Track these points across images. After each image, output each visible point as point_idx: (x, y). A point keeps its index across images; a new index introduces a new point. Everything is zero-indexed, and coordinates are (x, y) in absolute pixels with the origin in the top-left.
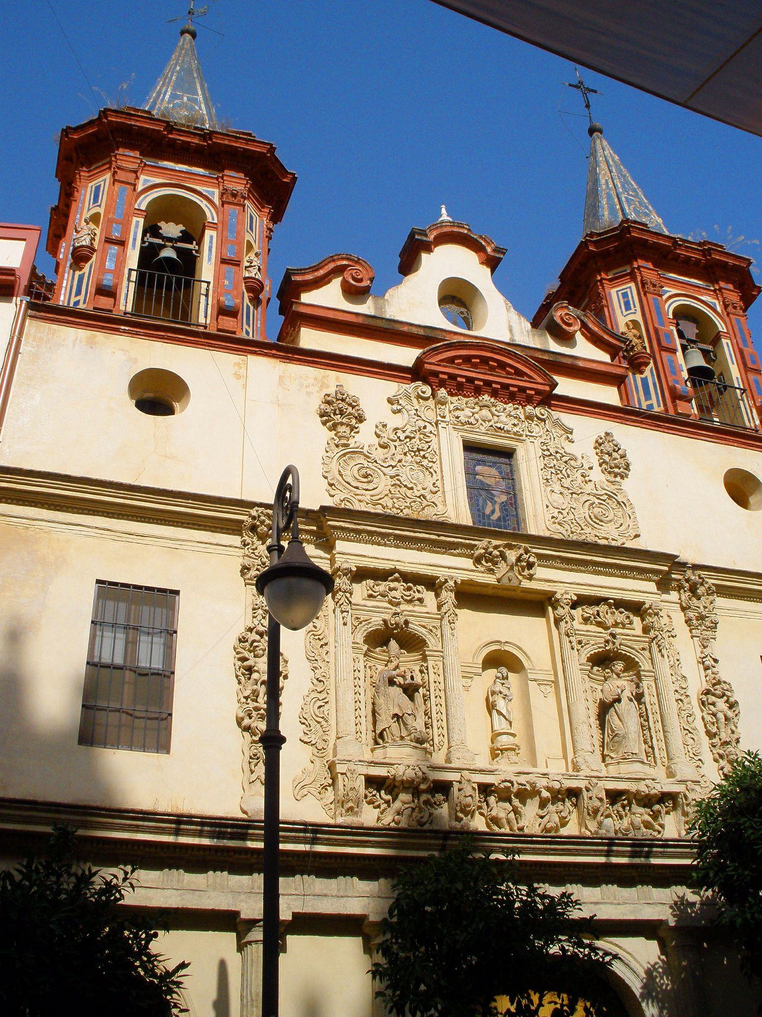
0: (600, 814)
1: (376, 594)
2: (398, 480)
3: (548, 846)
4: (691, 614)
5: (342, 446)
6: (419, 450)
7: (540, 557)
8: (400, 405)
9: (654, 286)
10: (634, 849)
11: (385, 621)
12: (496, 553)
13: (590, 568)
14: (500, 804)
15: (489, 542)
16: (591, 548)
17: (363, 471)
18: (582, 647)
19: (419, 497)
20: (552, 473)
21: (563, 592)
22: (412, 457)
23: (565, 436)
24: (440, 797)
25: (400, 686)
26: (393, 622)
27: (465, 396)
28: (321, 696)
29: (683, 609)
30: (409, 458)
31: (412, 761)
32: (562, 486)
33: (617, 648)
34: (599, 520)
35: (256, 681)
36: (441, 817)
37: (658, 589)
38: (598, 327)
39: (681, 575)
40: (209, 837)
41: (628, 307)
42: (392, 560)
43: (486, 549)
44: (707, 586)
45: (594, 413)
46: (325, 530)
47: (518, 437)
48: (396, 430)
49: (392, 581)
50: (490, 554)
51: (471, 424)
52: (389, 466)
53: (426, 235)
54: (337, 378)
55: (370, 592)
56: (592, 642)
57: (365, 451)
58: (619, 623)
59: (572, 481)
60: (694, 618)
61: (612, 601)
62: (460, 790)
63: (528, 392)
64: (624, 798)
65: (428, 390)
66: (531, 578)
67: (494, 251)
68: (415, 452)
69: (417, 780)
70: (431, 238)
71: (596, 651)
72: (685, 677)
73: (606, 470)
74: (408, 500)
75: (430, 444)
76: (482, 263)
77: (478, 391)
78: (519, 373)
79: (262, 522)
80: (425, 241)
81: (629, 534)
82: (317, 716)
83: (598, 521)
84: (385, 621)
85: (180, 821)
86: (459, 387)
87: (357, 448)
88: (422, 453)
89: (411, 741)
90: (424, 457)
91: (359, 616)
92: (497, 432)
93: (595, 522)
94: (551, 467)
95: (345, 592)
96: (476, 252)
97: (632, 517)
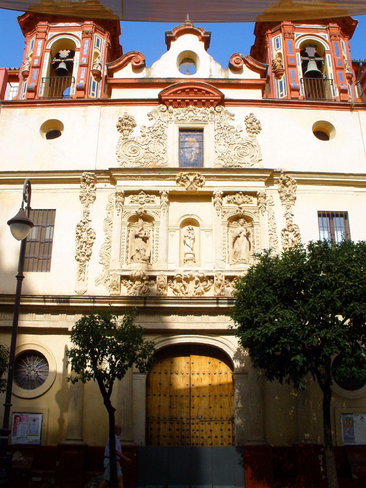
0: (221, 286)
1: (133, 201)
2: (149, 150)
3: (189, 301)
4: (282, 194)
6: (159, 135)
7: (206, 177)
8: (152, 116)
9: (289, 34)
10: (229, 301)
11: (136, 212)
12: (185, 178)
13: (231, 179)
14: (178, 283)
15: (182, 174)
19: (157, 156)
20: (221, 136)
21: (216, 191)
22: (156, 139)
24: (153, 282)
25: (141, 238)
27: (182, 107)
28: (108, 245)
30: (154, 139)
31: (140, 269)
35: (81, 242)
36: (154, 290)
37: (265, 185)
38: (253, 62)
40: (56, 302)
41: (278, 47)
44: (291, 181)
47: (205, 122)
49: (141, 194)
50: (182, 178)
51: (183, 120)
53: (172, 34)
56: (231, 211)
57: (135, 140)
58: (245, 202)
61: (241, 192)
62: (159, 279)
63: (211, 101)
64: (235, 279)
65: (165, 107)
66: (202, 186)
67: (205, 34)
68: (157, 136)
69: (141, 276)
70: (174, 34)
71: (232, 215)
73: (248, 131)
74: (152, 158)
75: (164, 132)
76: (200, 41)
77: (187, 104)
78: (208, 93)
79: (87, 178)
80: (171, 36)
83: (241, 156)
84: (136, 212)
85: (45, 298)
86: (177, 104)
87: (132, 139)
88: (160, 136)
90: (161, 138)
92: (195, 121)
93: (240, 156)
94: (221, 134)
95: (119, 202)
96: (198, 36)
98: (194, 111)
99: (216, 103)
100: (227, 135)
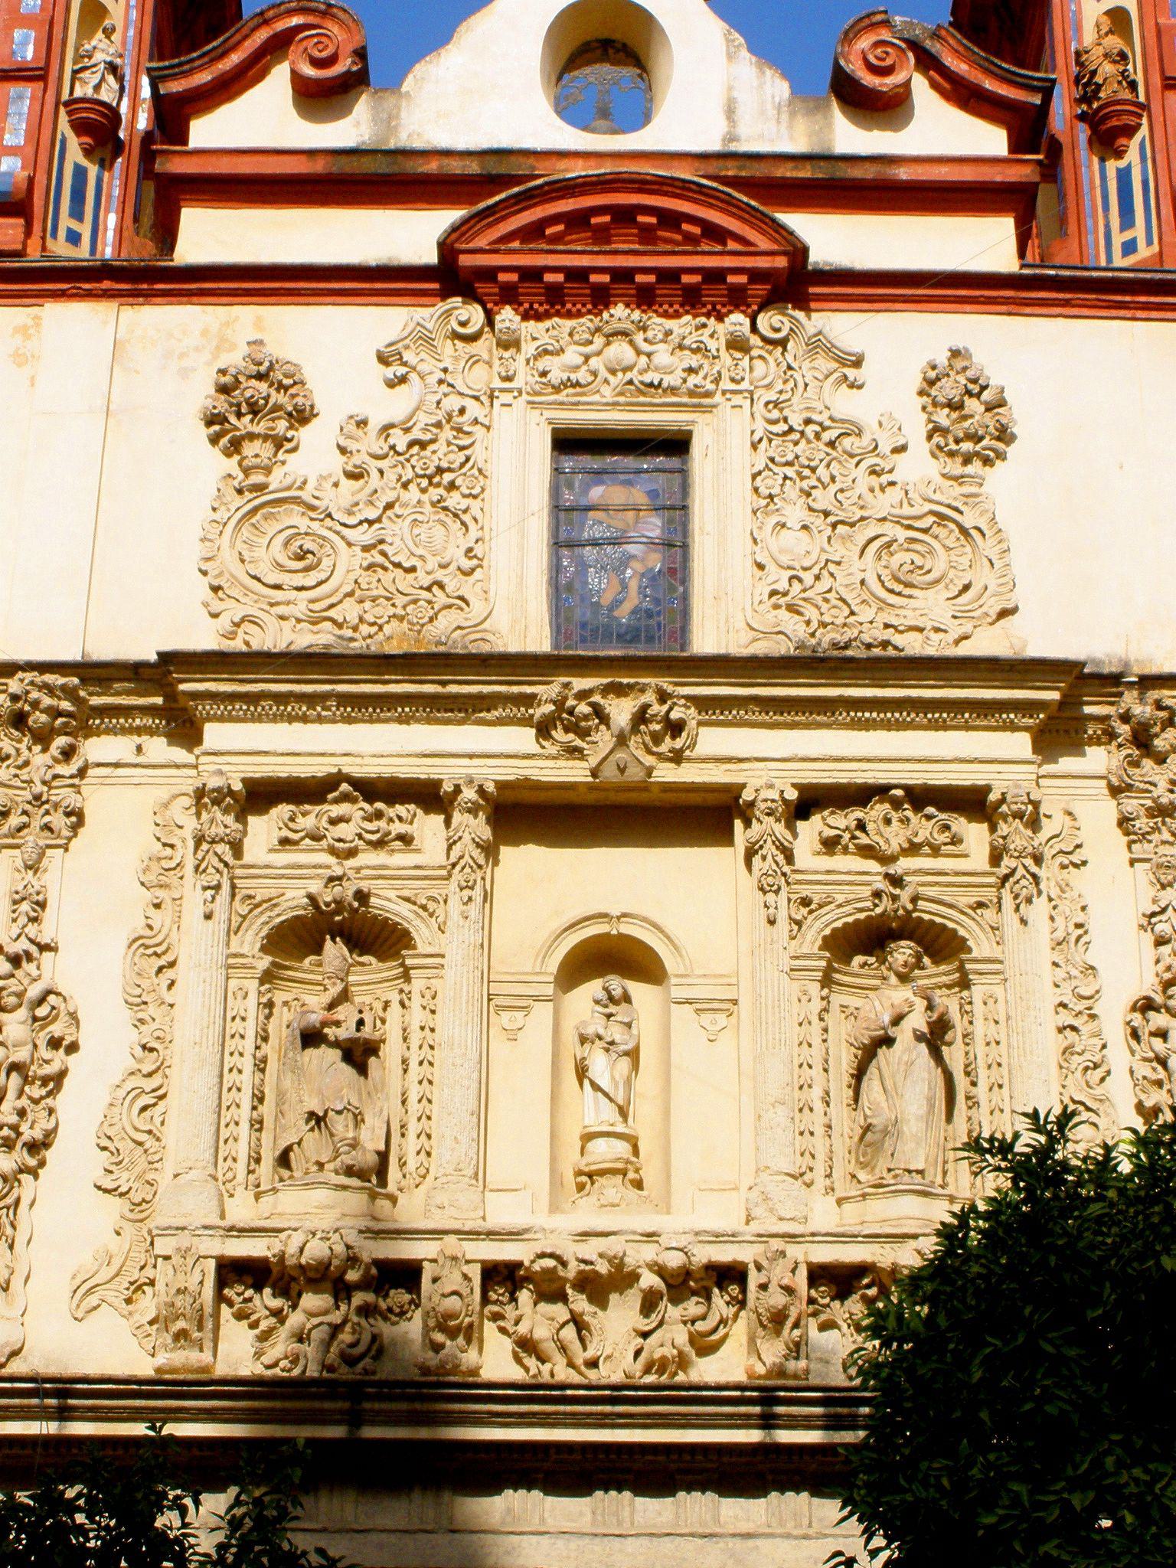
0: (789, 1323)
2: (384, 554)
3: (608, 1409)
5: (251, 491)
6: (440, 471)
7: (703, 704)
8: (405, 364)
10: (832, 1410)
11: (312, 898)
12: (583, 708)
14: (543, 1307)
15: (567, 685)
16: (836, 669)
17: (294, 546)
18: (811, 912)
19: (429, 589)
20: (786, 478)
23: (836, 375)
25: (336, 1044)
26: (328, 899)
27: (569, 315)
28: (149, 1084)
29: (1115, 791)
30: (414, 491)
31: (326, 1221)
32: (811, 509)
33: (904, 908)
34: (903, 584)
36: (406, 1342)
39: (1112, 704)
42: (332, 755)
43: (560, 703)
45: (930, 300)
46: (182, 702)
48: (387, 428)
49: (336, 801)
51: (578, 384)
52: (361, 523)
54: (258, 324)
55: (285, 833)
56: (840, 899)
57: (306, 495)
58: (920, 845)
59: (842, 491)
60: (1142, 812)
61: (899, 792)
62: (435, 1280)
64: (865, 1281)
65: (475, 314)
68: (430, 478)
69: (335, 1262)
71: (850, 919)
72: (1092, 968)
75: (467, 452)
77: (601, 299)
78: (715, 233)
79: (35, 704)
81: (984, 609)
82: (136, 1129)
83: (898, 588)
84: (312, 898)
87: (289, 488)
88: (447, 477)
89: (337, 1172)
90: (452, 486)
91: (251, 892)
92: (644, 394)
93: (891, 591)
95: (213, 842)
97: (998, 564)
98: (639, 338)
99: (761, 289)
100: (821, 471)
